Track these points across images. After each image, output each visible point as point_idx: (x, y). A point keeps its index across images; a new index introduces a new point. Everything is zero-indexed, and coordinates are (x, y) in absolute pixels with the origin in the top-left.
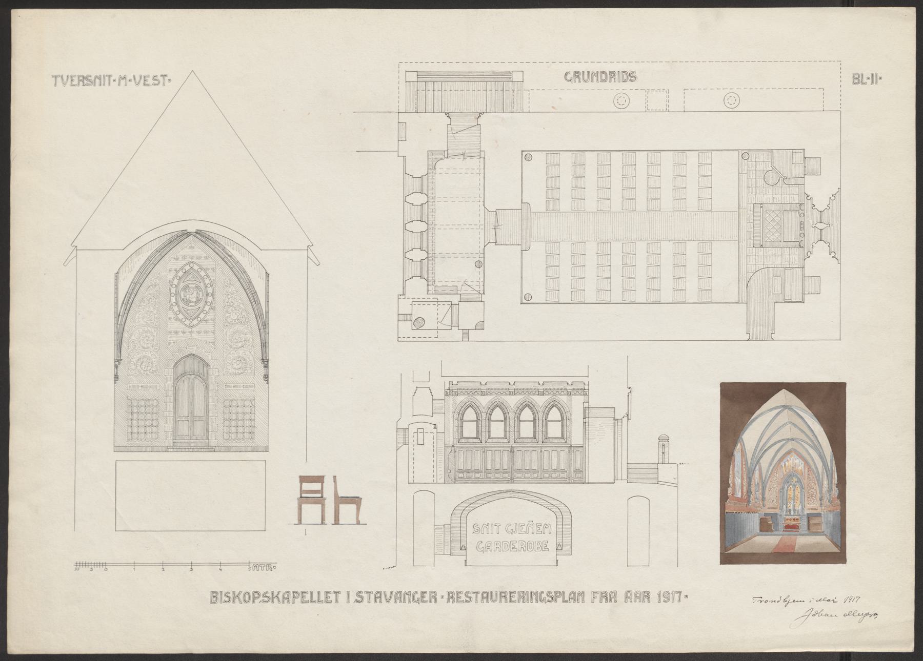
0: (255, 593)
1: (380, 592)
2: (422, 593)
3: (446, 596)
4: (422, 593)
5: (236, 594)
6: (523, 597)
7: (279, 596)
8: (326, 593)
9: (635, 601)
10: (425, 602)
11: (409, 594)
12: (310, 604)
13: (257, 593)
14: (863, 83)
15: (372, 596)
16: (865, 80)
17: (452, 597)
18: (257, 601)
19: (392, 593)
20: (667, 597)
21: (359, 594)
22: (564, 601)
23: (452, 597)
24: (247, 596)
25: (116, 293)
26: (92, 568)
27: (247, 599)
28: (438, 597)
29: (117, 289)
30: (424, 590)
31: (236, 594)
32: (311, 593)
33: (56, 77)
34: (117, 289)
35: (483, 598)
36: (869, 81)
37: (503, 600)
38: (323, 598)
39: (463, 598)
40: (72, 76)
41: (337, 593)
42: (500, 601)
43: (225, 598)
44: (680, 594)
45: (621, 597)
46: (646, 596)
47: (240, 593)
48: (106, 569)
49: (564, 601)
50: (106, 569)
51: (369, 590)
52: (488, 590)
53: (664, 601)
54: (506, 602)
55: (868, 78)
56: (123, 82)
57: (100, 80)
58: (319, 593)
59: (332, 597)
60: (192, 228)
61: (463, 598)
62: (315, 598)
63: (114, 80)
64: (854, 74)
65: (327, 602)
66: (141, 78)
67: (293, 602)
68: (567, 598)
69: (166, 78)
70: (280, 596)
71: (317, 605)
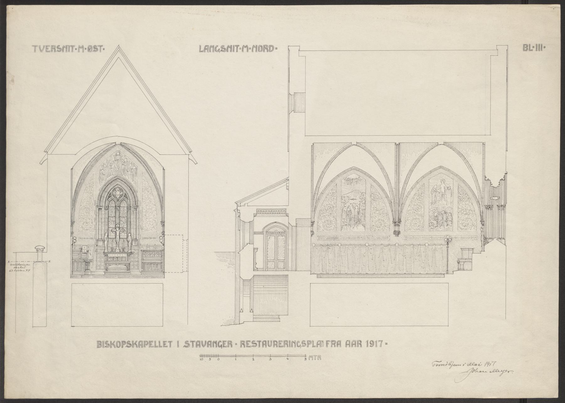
0: (123, 342)
4: (224, 342)
8: (164, 342)
10: (225, 347)
12: (154, 348)
14: (530, 50)
17: (243, 344)
18: (124, 346)
20: (372, 343)
21: (186, 342)
22: (313, 346)
23: (243, 344)
24: (118, 343)
25: (312, 180)
26: (210, 359)
27: (118, 346)
32: (155, 342)
33: (35, 46)
35: (263, 344)
36: (535, 49)
38: (162, 344)
39: (250, 344)
40: (47, 46)
41: (170, 342)
43: (105, 345)
44: (382, 342)
45: (343, 344)
46: (360, 343)
47: (114, 342)
48: (218, 359)
49: (313, 346)
50: (218, 359)
51: (193, 340)
52: (288, 340)
53: (371, 346)
54: (277, 347)
56: (81, 50)
57: (67, 48)
58: (159, 342)
59: (168, 344)
60: (441, 140)
61: (250, 344)
62: (157, 344)
63: (76, 49)
64: (524, 45)
65: (155, 347)
66: (44, 47)
68: (315, 344)
69: (102, 48)
71: (159, 348)
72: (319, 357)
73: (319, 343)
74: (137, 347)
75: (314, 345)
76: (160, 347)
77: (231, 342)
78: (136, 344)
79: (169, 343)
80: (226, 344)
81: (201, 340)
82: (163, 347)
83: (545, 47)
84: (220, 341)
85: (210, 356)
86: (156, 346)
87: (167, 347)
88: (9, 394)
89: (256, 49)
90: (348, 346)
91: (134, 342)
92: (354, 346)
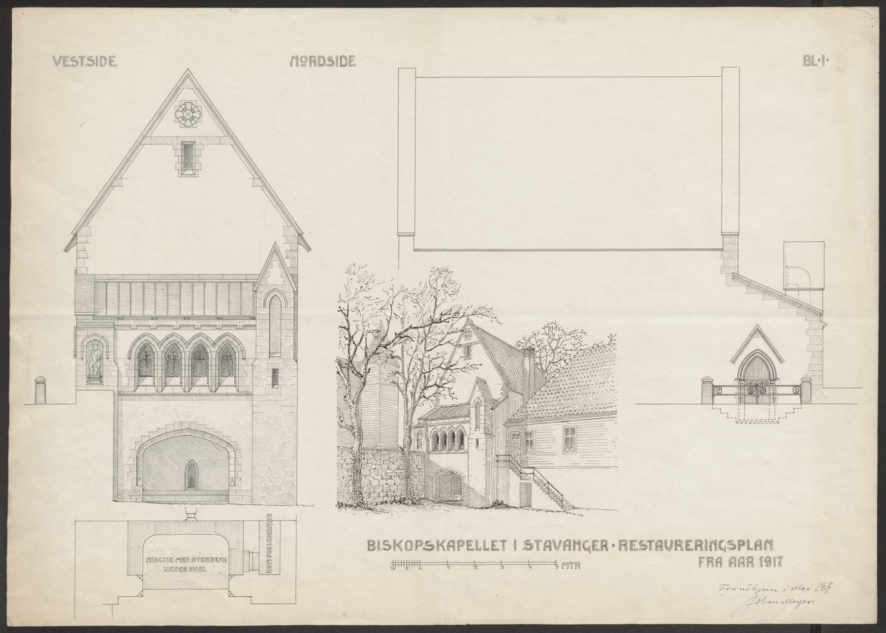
1: (660, 541)
2: (594, 541)
3: (617, 545)
4: (594, 541)
5: (397, 542)
6: (453, 546)
7: (443, 544)
9: (448, 550)
11: (715, 542)
13: (462, 541)
14: (814, 65)
15: (653, 544)
16: (816, 62)
18: (420, 549)
19: (560, 541)
21: (527, 542)
28: (609, 546)
29: (747, 343)
30: (596, 539)
31: (397, 542)
32: (477, 541)
34: (747, 343)
36: (820, 63)
37: (623, 548)
38: (489, 545)
39: (637, 545)
41: (504, 541)
42: (676, 549)
49: (749, 548)
52: (703, 539)
55: (819, 60)
59: (499, 545)
61: (637, 545)
62: (481, 545)
65: (493, 550)
67: (459, 550)
68: (752, 546)
70: (445, 545)
72: (578, 565)
73: (548, 544)
74: (444, 550)
75: (751, 547)
76: (486, 549)
77: (606, 542)
78: (442, 546)
79: (502, 543)
80: (599, 545)
81: (663, 539)
82: (490, 549)
83: (828, 60)
84: (587, 541)
85: (407, 564)
86: (478, 549)
87: (497, 550)
88: (14, 619)
89: (297, 60)
90: (451, 549)
91: (440, 542)
92: (548, 549)
